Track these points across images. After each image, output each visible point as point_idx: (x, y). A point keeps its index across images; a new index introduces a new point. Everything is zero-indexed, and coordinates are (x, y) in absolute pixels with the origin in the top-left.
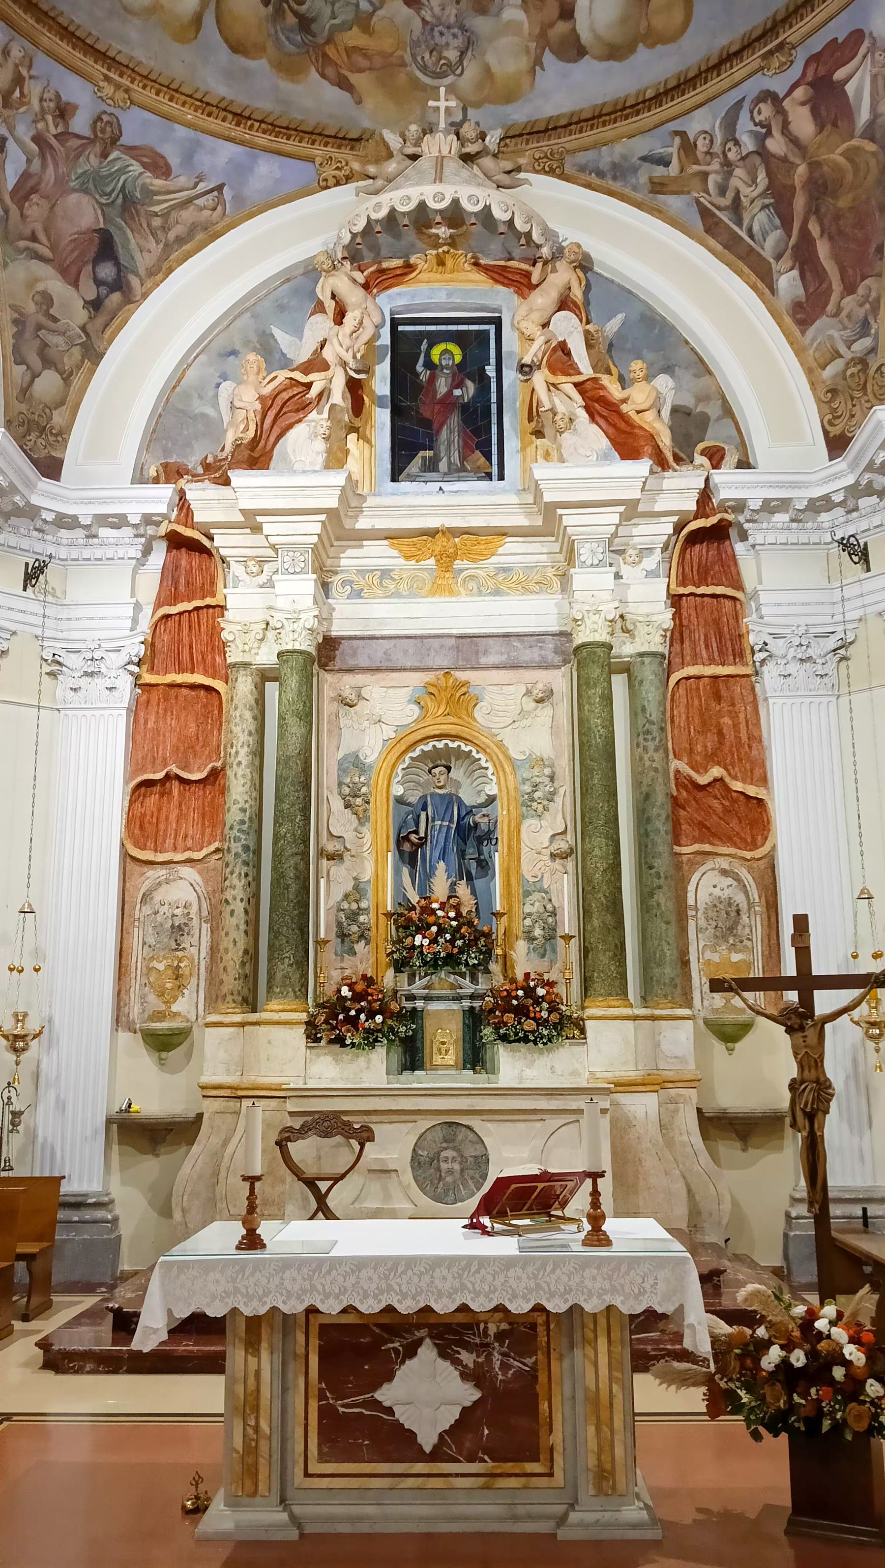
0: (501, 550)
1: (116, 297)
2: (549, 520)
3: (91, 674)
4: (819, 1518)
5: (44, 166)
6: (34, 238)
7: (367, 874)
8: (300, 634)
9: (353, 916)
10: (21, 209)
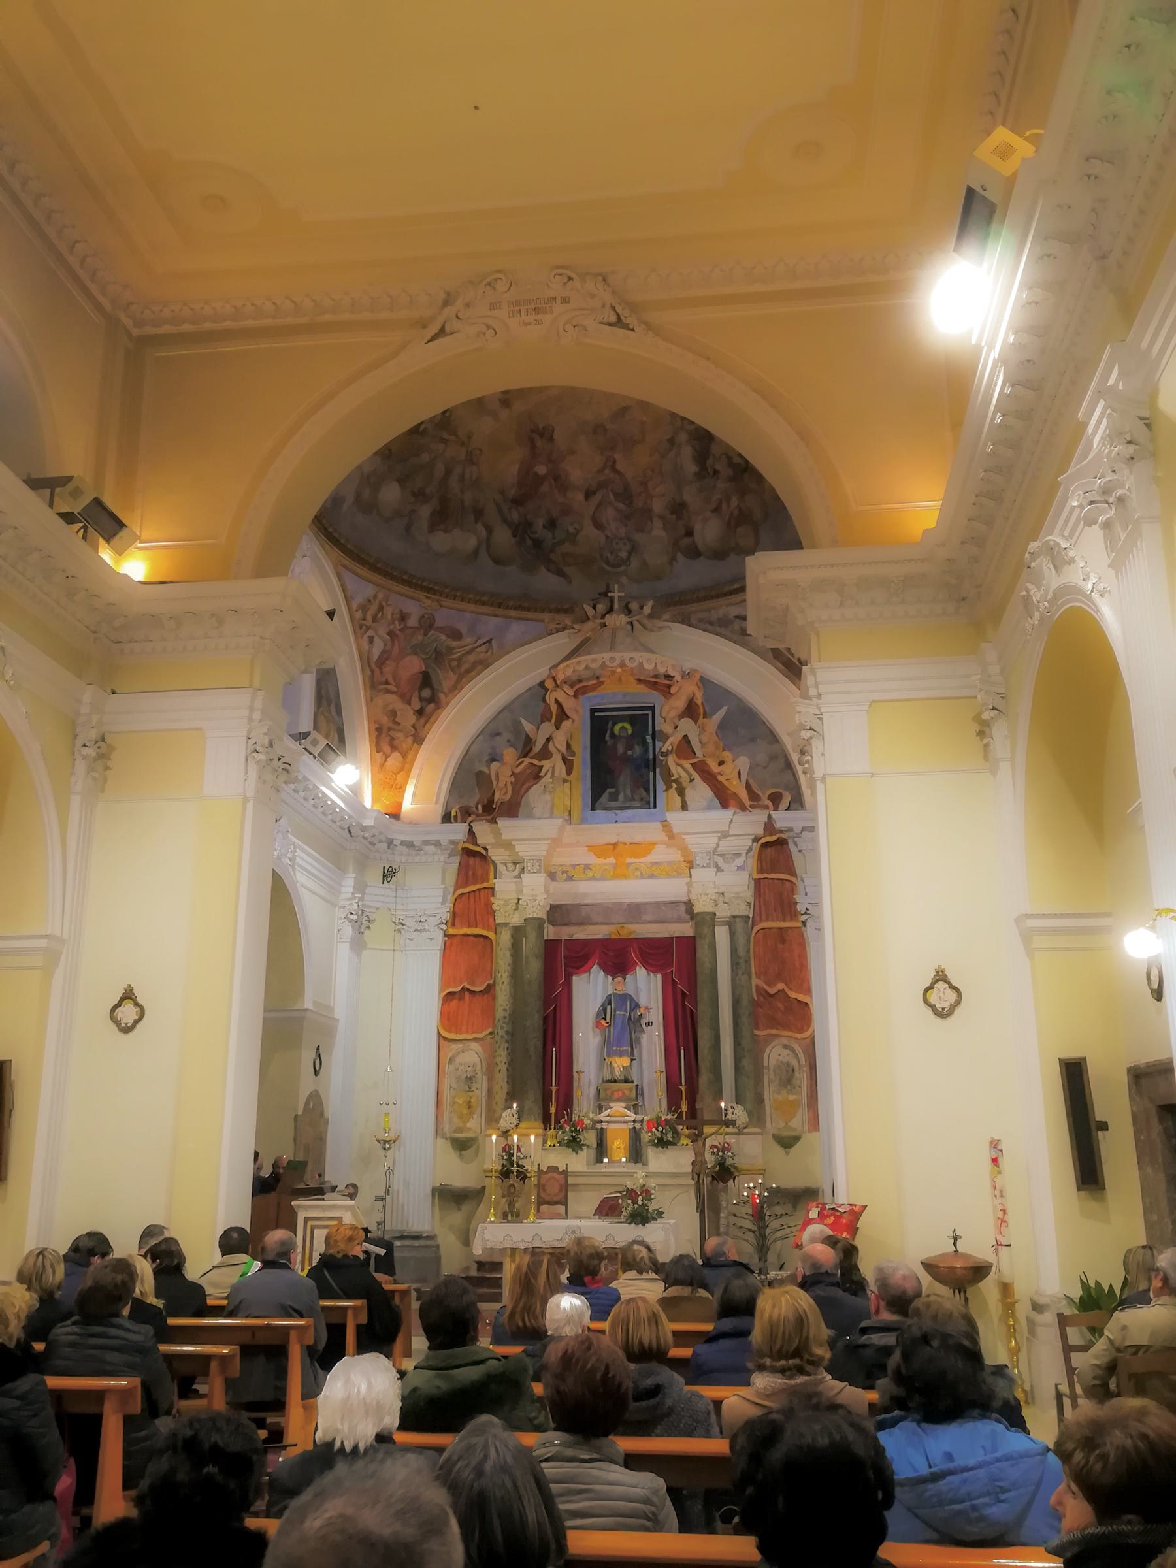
1: (432, 705)
3: (420, 931)
4: (1029, 1560)
5: (393, 645)
6: (387, 683)
10: (380, 669)
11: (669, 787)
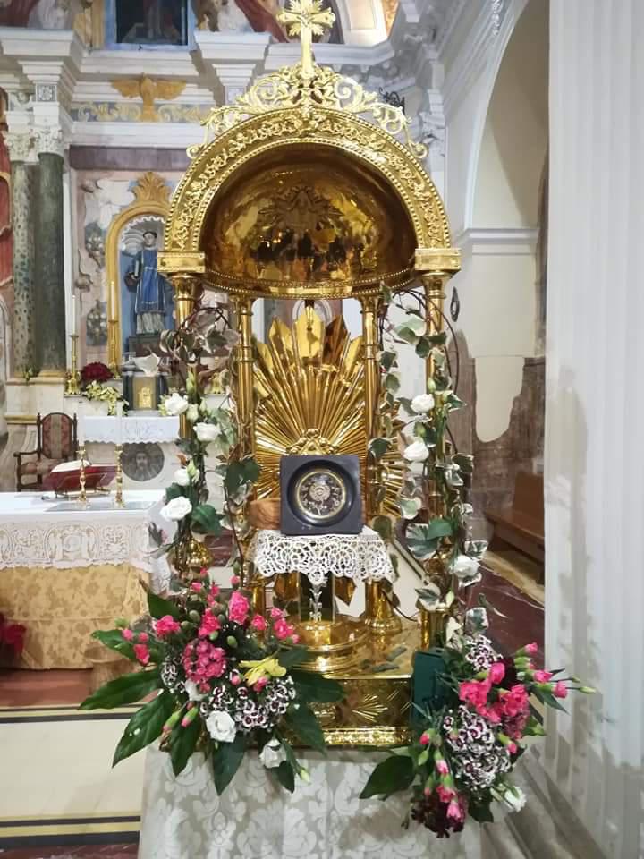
0: (183, 93)
2: (205, 71)
7: (104, 299)
8: (51, 143)
9: (96, 322)
11: (201, 20)
